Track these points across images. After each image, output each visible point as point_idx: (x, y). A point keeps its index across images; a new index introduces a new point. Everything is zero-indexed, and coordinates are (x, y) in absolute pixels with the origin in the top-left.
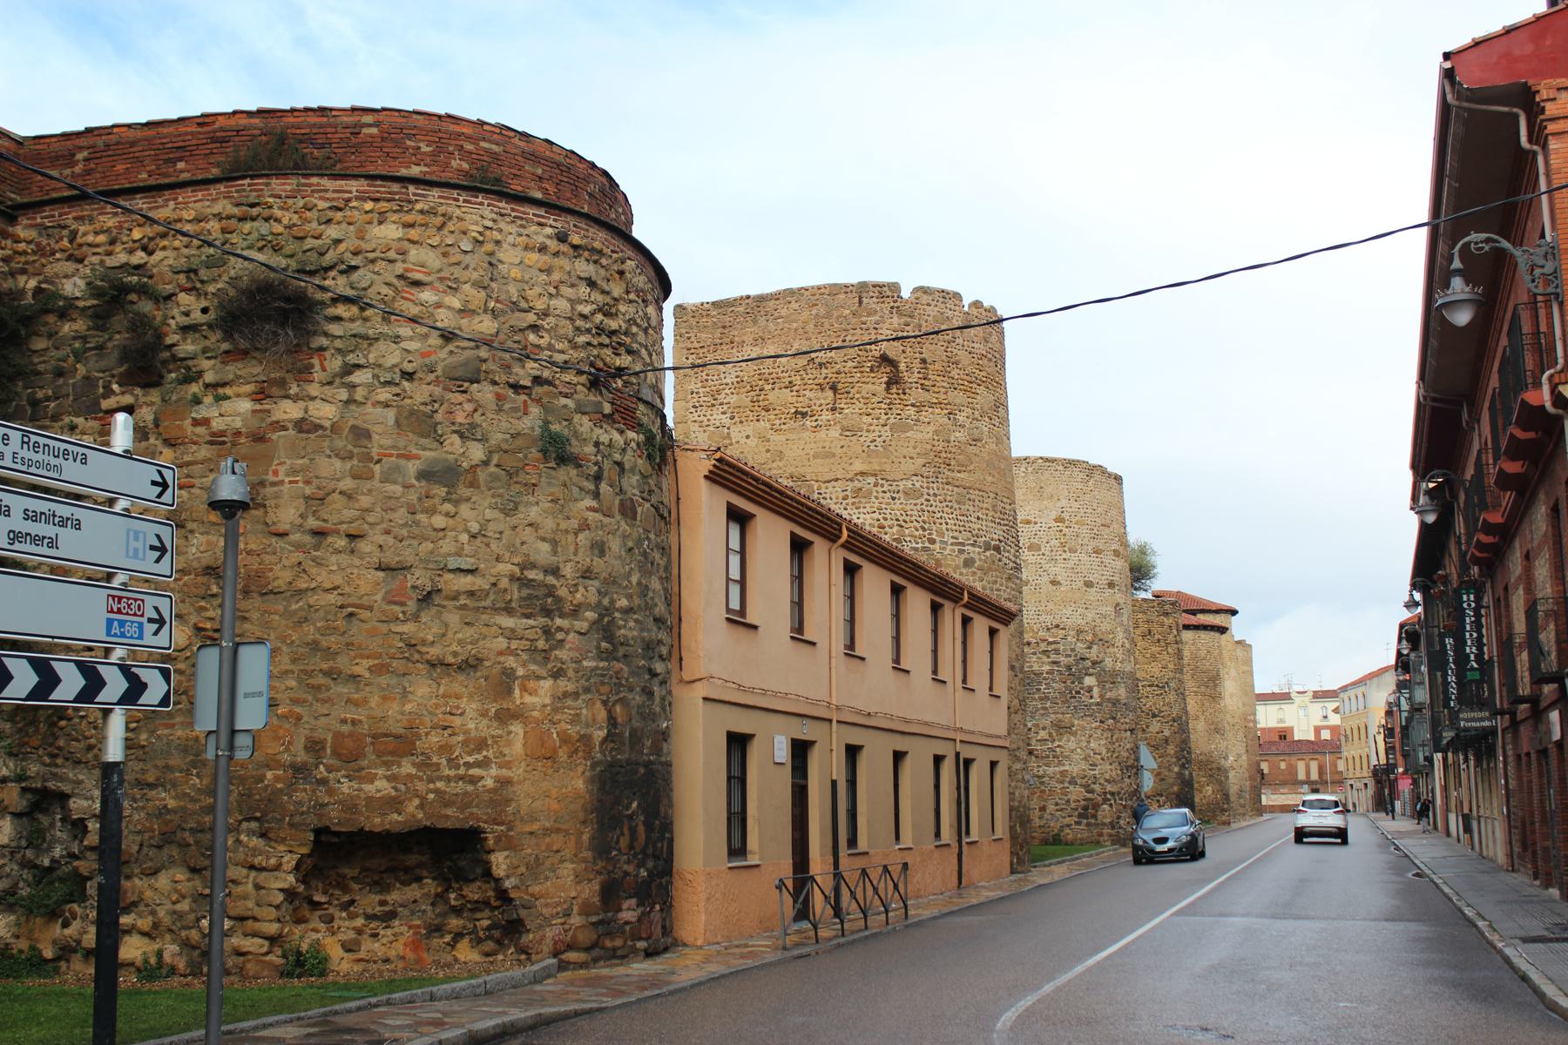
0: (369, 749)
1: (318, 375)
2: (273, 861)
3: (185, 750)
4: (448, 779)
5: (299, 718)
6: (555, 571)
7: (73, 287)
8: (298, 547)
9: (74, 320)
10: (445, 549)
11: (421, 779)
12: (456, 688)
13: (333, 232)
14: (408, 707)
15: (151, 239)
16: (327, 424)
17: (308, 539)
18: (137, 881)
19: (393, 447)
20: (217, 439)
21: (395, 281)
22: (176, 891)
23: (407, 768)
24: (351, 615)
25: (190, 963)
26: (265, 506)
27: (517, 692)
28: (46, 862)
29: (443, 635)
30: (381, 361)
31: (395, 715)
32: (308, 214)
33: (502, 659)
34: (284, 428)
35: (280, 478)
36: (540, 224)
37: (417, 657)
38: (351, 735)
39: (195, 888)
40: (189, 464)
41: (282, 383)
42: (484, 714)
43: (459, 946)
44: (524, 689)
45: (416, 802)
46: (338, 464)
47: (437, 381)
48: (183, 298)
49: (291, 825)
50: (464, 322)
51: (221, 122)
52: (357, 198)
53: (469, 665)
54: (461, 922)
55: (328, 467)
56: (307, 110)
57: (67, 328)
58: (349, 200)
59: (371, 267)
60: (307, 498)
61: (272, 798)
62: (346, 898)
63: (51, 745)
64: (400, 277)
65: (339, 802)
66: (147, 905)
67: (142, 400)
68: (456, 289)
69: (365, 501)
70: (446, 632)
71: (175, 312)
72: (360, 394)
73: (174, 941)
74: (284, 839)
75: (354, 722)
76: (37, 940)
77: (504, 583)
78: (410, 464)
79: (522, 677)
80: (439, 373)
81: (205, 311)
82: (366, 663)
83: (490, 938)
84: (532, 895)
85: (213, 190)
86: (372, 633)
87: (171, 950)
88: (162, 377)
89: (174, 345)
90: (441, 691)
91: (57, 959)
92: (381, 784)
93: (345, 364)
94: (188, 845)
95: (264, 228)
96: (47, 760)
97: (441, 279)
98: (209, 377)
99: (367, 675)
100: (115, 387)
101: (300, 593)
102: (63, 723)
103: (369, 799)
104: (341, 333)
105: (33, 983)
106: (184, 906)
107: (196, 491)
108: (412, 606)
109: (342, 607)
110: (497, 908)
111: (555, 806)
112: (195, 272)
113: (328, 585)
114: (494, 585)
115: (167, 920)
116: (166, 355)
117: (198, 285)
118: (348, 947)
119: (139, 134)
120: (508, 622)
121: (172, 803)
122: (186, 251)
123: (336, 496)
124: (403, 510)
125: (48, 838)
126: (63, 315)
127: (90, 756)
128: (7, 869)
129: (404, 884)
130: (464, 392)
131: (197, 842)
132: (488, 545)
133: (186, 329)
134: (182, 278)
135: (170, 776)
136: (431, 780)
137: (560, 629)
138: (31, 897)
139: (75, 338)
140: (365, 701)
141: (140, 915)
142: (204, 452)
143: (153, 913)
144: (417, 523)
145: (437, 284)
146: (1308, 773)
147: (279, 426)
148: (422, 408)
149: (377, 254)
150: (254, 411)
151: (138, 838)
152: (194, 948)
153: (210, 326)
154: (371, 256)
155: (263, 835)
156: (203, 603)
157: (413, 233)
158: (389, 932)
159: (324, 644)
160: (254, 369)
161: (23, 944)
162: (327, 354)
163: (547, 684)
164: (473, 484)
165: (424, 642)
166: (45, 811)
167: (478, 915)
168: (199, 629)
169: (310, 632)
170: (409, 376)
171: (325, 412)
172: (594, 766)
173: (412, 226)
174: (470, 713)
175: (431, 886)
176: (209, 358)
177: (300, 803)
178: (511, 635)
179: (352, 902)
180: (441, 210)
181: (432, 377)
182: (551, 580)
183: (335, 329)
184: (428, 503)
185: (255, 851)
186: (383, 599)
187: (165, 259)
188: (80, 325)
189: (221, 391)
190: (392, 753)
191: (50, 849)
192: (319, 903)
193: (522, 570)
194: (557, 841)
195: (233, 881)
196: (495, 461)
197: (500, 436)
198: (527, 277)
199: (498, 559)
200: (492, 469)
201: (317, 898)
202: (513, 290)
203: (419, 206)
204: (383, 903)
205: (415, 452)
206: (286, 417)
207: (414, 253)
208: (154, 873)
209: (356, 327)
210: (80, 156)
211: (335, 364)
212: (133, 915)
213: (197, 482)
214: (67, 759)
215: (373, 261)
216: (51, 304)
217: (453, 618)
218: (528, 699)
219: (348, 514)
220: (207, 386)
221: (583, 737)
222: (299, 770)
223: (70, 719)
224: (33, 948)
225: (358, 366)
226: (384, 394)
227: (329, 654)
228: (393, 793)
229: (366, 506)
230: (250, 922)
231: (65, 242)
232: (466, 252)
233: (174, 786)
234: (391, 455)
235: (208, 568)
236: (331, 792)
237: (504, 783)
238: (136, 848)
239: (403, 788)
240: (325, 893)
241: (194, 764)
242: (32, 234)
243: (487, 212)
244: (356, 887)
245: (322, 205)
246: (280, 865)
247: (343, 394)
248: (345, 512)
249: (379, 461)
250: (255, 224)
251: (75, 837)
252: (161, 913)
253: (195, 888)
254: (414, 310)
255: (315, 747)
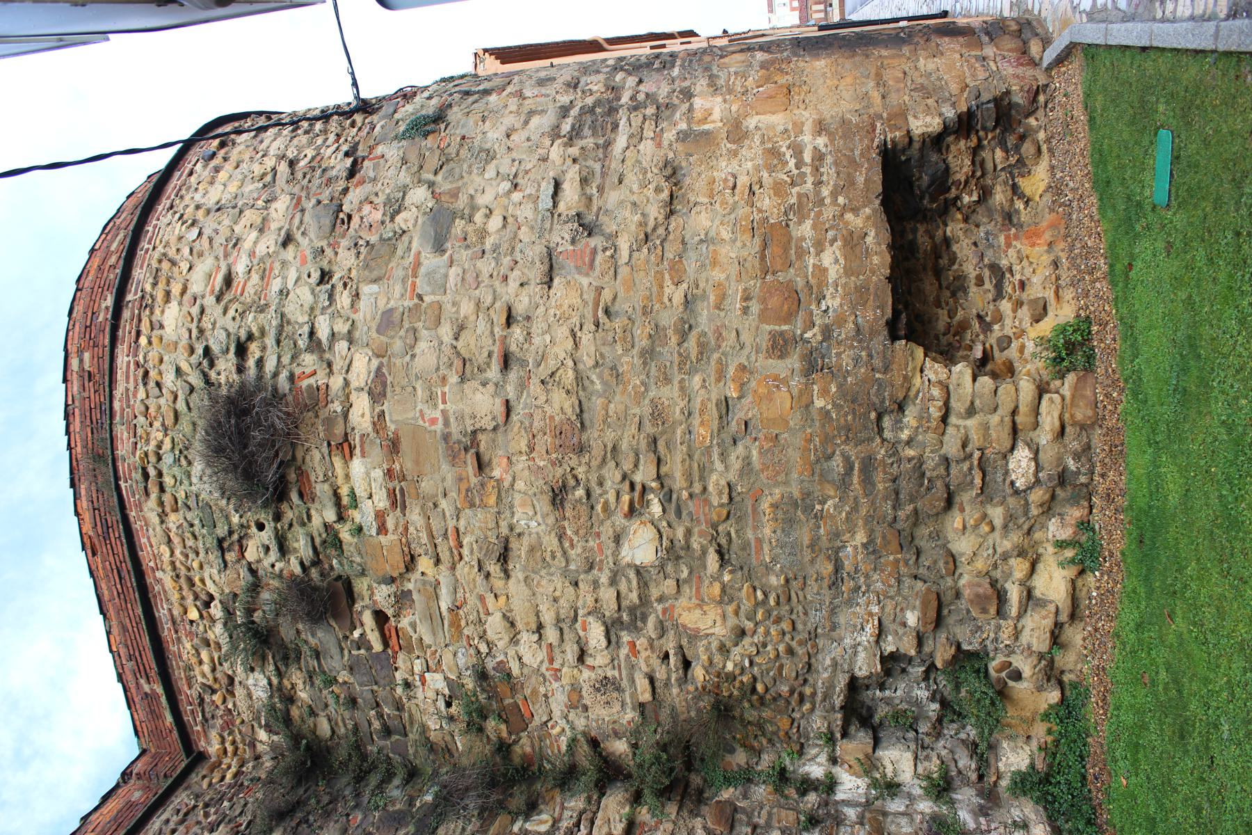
0: (781, 277)
1: (321, 379)
2: (936, 392)
3: (790, 522)
4: (818, 183)
5: (743, 368)
6: (564, 111)
7: (256, 685)
8: (522, 386)
9: (293, 686)
10: (530, 215)
11: (820, 214)
12: (701, 185)
13: (169, 379)
14: (725, 234)
15: (196, 597)
16: (375, 362)
17: (513, 375)
18: (962, 582)
19: (404, 281)
20: (397, 500)
21: (223, 303)
22: (976, 526)
23: (805, 230)
24: (607, 312)
25: (1074, 501)
26: (474, 432)
27: (706, 127)
28: (935, 706)
29: (635, 204)
30: (307, 307)
31: (735, 250)
32: (152, 410)
33: (665, 143)
34: (382, 415)
35: (438, 414)
36: (191, 174)
37: (661, 231)
38: (763, 301)
39: (973, 501)
40: (431, 536)
41: (329, 422)
42: (735, 154)
43: (1028, 192)
44: (704, 120)
45: (849, 216)
46: (422, 346)
47: (334, 246)
48: (251, 554)
49: (886, 369)
50: (274, 226)
51: (87, 528)
52: (136, 355)
53: (673, 173)
54: (998, 188)
55: (426, 356)
56: (68, 432)
57: (303, 695)
58: (137, 364)
59: (208, 333)
60: (463, 379)
61: (850, 397)
62: (976, 325)
63: (788, 703)
64: (218, 299)
65: (853, 308)
66: (995, 566)
67: (367, 601)
68: (238, 240)
69: (467, 308)
70: (629, 204)
71: (266, 563)
72: (342, 327)
73: (1044, 527)
74: (906, 378)
75: (747, 298)
76: (1035, 713)
77: (574, 151)
78: (425, 262)
79: (689, 124)
80: (324, 243)
81: (261, 527)
82: (669, 288)
83: (1017, 148)
84: (962, 90)
85: (137, 526)
86: (631, 284)
87: (1056, 529)
88: (339, 577)
89: (302, 564)
90: (705, 200)
91: (1061, 683)
92: (827, 259)
93: (309, 349)
94: (916, 511)
95: (168, 459)
96: (807, 706)
97: (226, 256)
98: (330, 515)
99: (685, 286)
100: (356, 634)
101: (579, 379)
102: (760, 688)
103: (848, 272)
104: (275, 358)
105: (1093, 711)
106: (997, 514)
107: (462, 524)
108: (596, 241)
109: (597, 325)
110: (980, 140)
111: (849, 80)
112: (220, 541)
113: (569, 344)
114: (574, 161)
115: (1015, 537)
116: (314, 573)
117: (235, 537)
118: (1040, 313)
119: (114, 623)
120: (621, 141)
121: (861, 537)
122: (202, 554)
123: (460, 345)
124: (479, 264)
125: (904, 706)
126: (290, 699)
127: (800, 651)
128: (944, 753)
129: (953, 259)
130: (350, 217)
131: (912, 500)
132: (527, 172)
133: (283, 550)
134: (231, 556)
135: (824, 542)
136: (821, 202)
137: (633, 98)
138: (979, 725)
139: (312, 684)
140: (718, 286)
141: (1008, 575)
142: (415, 516)
143: (1005, 557)
144: (496, 248)
145: (231, 260)
146: (820, 11)
147: (379, 421)
148: (362, 257)
149: (194, 326)
150: (363, 456)
151: (908, 581)
152: (1053, 497)
153: (278, 517)
154: (195, 333)
155: (901, 408)
156: (599, 508)
157: (176, 289)
158: (1016, 268)
159: (645, 342)
160: (315, 459)
161: (1039, 730)
162: (298, 371)
163: (698, 102)
164: (455, 195)
165: (643, 224)
166: (871, 712)
167: (989, 166)
168: (632, 512)
169: (629, 362)
170: (325, 276)
171: (362, 367)
172: (796, 55)
173: (168, 294)
174: (734, 166)
175: (954, 228)
176: (309, 517)
177: (856, 361)
178: (637, 137)
179: (980, 317)
180: (155, 265)
181: (329, 252)
182: (574, 112)
183: (270, 366)
184: (472, 238)
185: (923, 416)
186: (587, 275)
187: (215, 580)
188: (296, 677)
189: (345, 501)
190: (786, 250)
191: (918, 703)
192: (984, 351)
193: (559, 137)
194: (888, 75)
195: (964, 446)
196: (430, 177)
197: (403, 173)
198: (240, 177)
199: (544, 159)
200: (439, 178)
201: (979, 355)
202: (249, 187)
203: (148, 288)
204: (980, 281)
205: (411, 259)
206: (368, 417)
207: (196, 287)
208: (953, 558)
209: (270, 341)
210: (146, 688)
211: (309, 360)
212: (1008, 586)
213: (451, 524)
214: (805, 681)
215: (201, 331)
216: (281, 711)
217: (613, 197)
218: (717, 115)
219: (482, 326)
220: (341, 518)
221: (762, 67)
222: (813, 365)
223: (755, 679)
224: (1046, 717)
225: (312, 333)
226: (343, 299)
227: (657, 334)
228: (839, 243)
229: (472, 306)
230: (1019, 419)
231: (217, 698)
232: (200, 234)
233: (837, 535)
234: (414, 284)
235: (553, 502)
236: (841, 321)
237: (821, 127)
238: (920, 584)
239: (830, 234)
240: (970, 348)
241: (808, 509)
242: (213, 734)
243: (165, 220)
244: (960, 315)
245: (141, 394)
246: (940, 382)
247: (342, 346)
248: (479, 331)
249: (420, 298)
250: (165, 472)
251: (904, 671)
252: (1006, 545)
253: (973, 501)
254: (255, 278)
255: (780, 346)
